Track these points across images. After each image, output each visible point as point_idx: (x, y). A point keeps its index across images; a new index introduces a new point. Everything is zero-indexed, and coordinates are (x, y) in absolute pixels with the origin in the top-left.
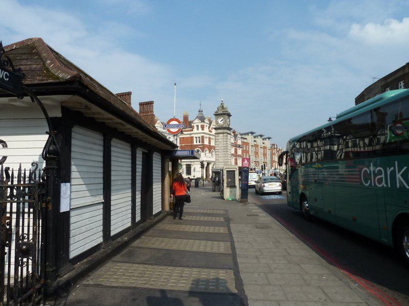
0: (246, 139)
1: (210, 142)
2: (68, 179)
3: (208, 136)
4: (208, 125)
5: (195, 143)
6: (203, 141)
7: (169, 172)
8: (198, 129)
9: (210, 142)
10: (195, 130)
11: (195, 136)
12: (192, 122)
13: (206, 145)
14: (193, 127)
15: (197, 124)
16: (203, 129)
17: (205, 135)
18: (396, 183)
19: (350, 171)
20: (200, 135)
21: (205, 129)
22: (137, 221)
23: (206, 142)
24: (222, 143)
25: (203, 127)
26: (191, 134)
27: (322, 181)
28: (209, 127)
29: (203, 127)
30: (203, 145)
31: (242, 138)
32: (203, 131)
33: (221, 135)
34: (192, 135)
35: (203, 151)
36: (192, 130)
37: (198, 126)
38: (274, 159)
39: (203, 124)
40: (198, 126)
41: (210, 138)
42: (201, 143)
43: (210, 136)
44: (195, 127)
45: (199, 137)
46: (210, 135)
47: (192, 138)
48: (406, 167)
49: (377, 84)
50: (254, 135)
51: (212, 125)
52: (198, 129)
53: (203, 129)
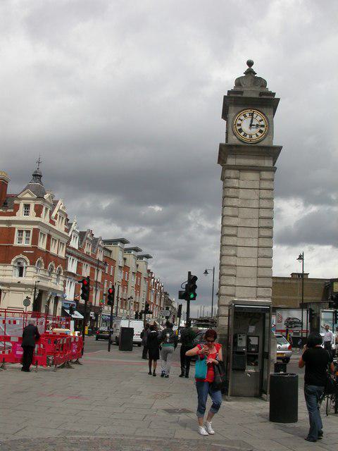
0: (110, 252)
1: (48, 246)
2: (225, 96)
5: (16, 243)
6: (35, 241)
8: (27, 213)
9: (48, 246)
10: (20, 215)
12: (15, 197)
13: (41, 251)
14: (16, 207)
15: (27, 202)
16: (38, 215)
20: (31, 227)
21: (43, 215)
22: (82, 317)
24: (255, 204)
25: (38, 211)
26: (9, 222)
29: (38, 211)
30: (35, 249)
31: (105, 249)
32: (38, 219)
33: (252, 176)
34: (13, 226)
35: (32, 263)
36: (14, 214)
37: (27, 206)
39: (39, 202)
40: (27, 206)
42: (29, 245)
43: (51, 233)
44: (22, 207)
45: (28, 232)
48: (188, 353)
50: (126, 246)
52: (27, 213)
53: (38, 215)
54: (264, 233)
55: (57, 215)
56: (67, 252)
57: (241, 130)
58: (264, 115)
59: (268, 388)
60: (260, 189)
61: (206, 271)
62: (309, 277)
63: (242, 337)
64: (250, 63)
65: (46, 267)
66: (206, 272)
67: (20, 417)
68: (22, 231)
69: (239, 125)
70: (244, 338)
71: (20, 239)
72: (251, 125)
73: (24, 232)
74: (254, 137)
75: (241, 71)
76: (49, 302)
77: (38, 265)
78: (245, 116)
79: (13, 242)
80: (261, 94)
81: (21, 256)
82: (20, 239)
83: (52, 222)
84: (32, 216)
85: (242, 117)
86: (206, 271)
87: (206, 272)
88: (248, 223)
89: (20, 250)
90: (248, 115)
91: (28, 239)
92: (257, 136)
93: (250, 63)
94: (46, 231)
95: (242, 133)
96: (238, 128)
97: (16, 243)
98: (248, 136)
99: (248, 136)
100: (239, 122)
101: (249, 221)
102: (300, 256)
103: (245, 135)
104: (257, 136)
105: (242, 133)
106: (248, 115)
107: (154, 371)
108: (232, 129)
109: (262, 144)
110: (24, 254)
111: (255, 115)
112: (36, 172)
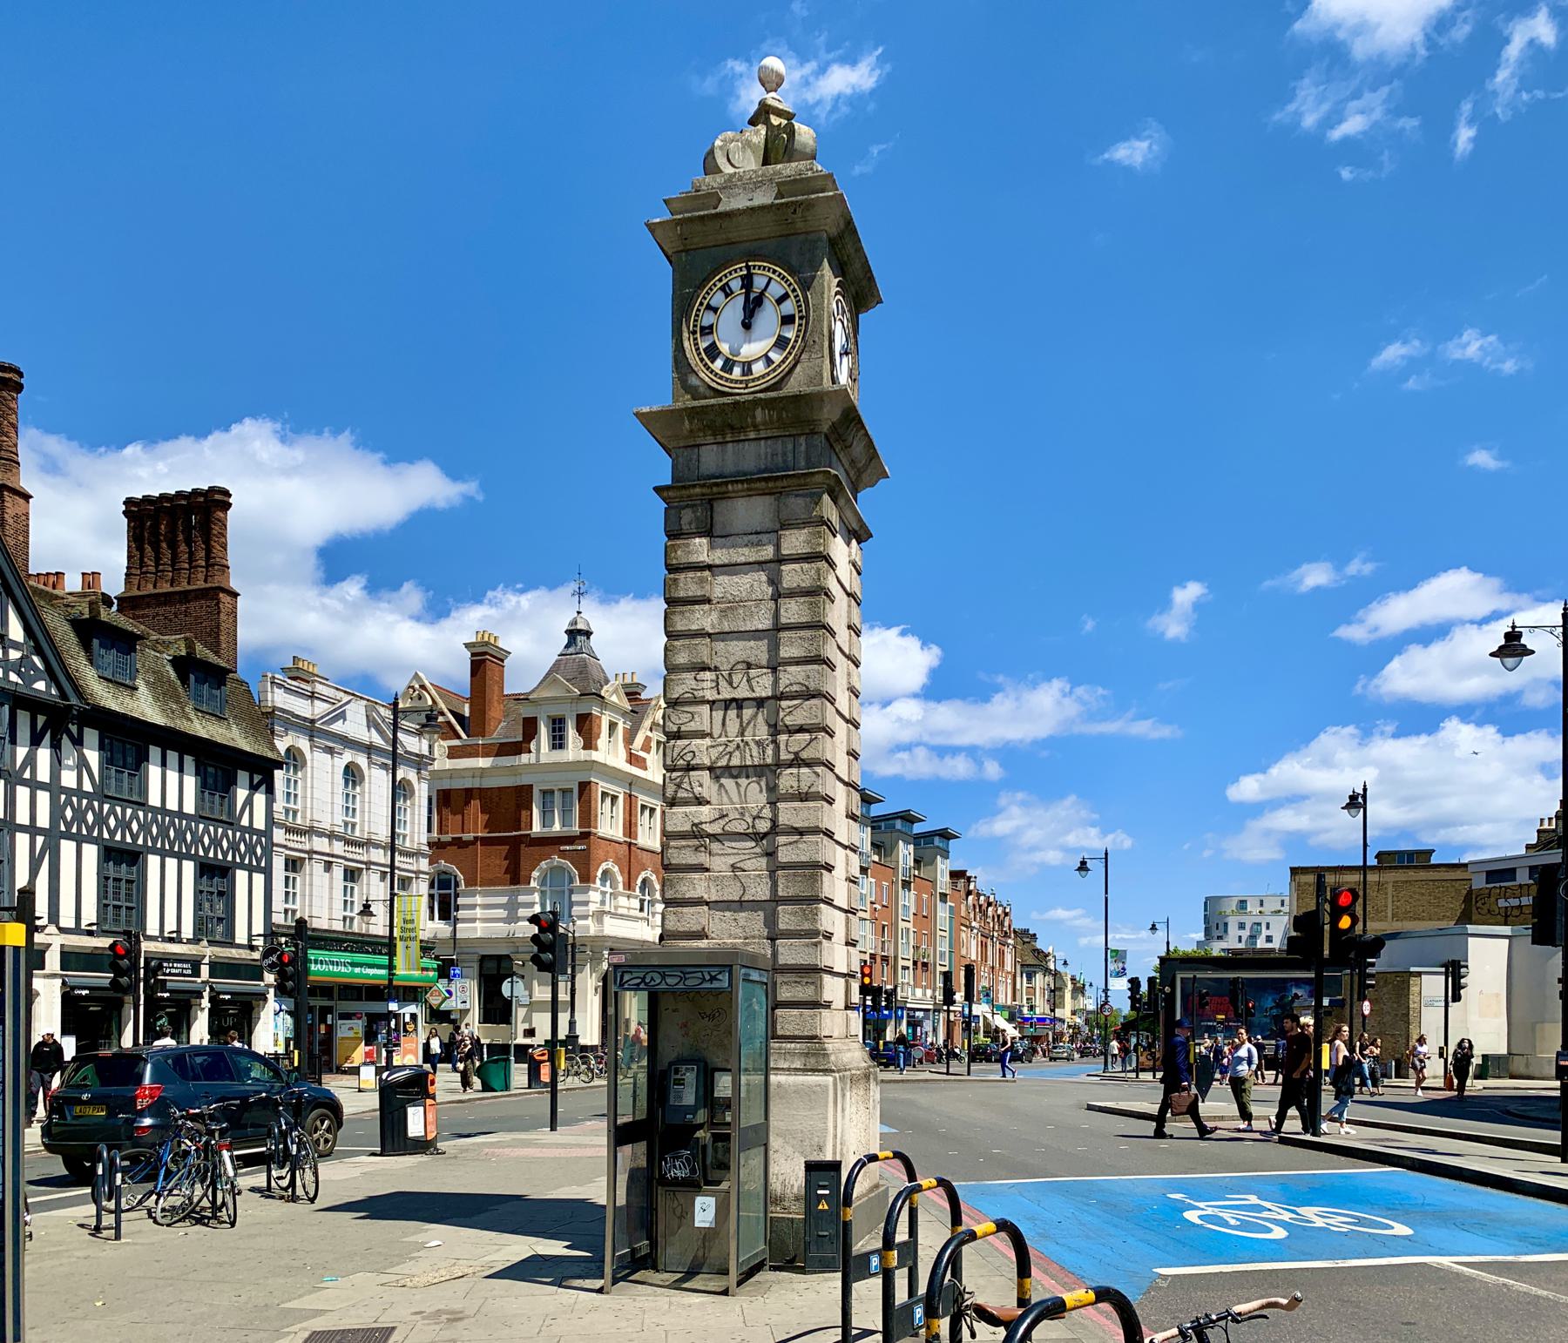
1: (630, 828)
6: (587, 817)
8: (558, 742)
9: (630, 828)
15: (556, 711)
16: (589, 744)
21: (602, 742)
34: (525, 781)
42: (576, 829)
52: (558, 742)
53: (589, 744)
55: (648, 739)
61: (1083, 863)
65: (629, 885)
68: (552, 792)
69: (708, 330)
73: (557, 795)
77: (642, 890)
78: (727, 291)
83: (633, 759)
84: (574, 748)
85: (718, 299)
97: (537, 828)
102: (1353, 798)
106: (736, 285)
107: (572, 1024)
109: (793, 386)
110: (563, 854)
111: (759, 283)
112: (575, 622)
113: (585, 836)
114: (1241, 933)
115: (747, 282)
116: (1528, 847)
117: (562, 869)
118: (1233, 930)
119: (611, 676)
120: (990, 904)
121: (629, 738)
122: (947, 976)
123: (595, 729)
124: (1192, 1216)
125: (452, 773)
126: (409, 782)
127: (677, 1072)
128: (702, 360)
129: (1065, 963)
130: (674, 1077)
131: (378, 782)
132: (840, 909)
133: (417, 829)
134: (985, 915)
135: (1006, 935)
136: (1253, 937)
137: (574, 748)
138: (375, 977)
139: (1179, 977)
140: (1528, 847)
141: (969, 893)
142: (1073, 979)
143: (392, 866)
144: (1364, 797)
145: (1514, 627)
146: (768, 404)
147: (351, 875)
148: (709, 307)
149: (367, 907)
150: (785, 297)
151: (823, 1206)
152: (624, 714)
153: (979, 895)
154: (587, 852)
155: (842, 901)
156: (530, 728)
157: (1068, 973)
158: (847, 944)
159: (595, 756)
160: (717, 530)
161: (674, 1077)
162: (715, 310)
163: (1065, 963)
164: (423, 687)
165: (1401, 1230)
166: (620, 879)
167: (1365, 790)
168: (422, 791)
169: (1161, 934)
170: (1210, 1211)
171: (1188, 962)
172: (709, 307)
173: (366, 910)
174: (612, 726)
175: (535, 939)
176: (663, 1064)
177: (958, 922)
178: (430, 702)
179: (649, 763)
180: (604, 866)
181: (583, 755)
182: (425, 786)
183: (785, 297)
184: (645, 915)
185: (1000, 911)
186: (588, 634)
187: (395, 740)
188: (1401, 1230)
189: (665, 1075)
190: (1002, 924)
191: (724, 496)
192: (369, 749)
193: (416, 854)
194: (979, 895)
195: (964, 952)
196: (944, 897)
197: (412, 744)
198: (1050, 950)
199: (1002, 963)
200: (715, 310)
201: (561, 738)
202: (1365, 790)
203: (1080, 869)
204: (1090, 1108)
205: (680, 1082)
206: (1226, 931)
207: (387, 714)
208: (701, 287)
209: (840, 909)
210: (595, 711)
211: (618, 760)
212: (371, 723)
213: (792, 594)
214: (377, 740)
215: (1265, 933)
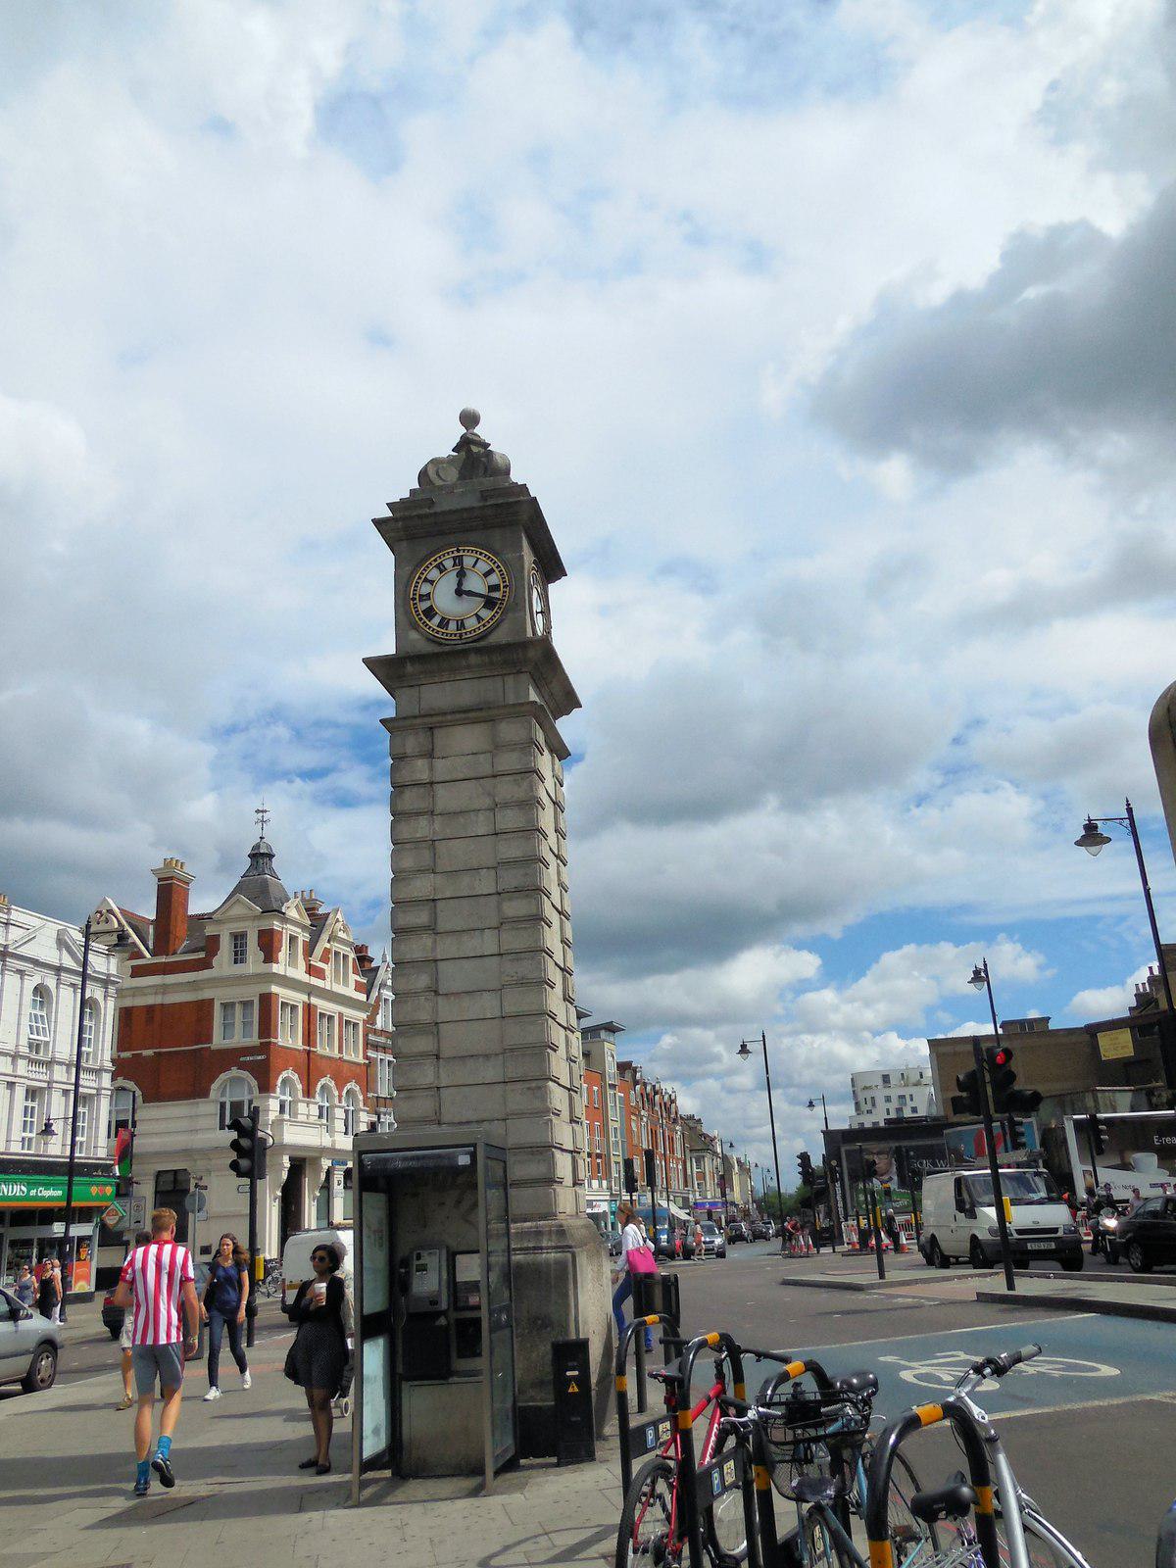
3: (298, 998)
4: (303, 937)
5: (218, 1041)
6: (266, 1027)
7: (351, 1336)
8: (239, 956)
9: (309, 1038)
11: (219, 995)
15: (238, 927)
17: (322, 1005)
18: (109, 1483)
19: (321, 1039)
20: (252, 993)
21: (283, 955)
23: (287, 1037)
26: (194, 985)
27: (517, 1386)
28: (309, 950)
34: (206, 994)
36: (205, 964)
38: (635, 1142)
40: (239, 939)
41: (309, 1008)
42: (254, 1040)
43: (314, 1001)
45: (247, 1004)
46: (311, 990)
47: (204, 1008)
49: (1061, 1033)
51: (325, 936)
52: (239, 956)
53: (270, 957)
54: (515, 908)
56: (367, 1044)
57: (430, 613)
58: (496, 554)
59: (1085, 1363)
60: (495, 776)
61: (744, 1046)
62: (1052, 1026)
63: (426, 1259)
64: (469, 419)
66: (744, 1050)
67: (431, 1528)
68: (233, 1004)
70: (434, 1261)
71: (228, 1027)
72: (459, 592)
73: (238, 1008)
74: (471, 624)
75: (444, 442)
76: (327, 1187)
78: (441, 568)
79: (209, 1039)
80: (484, 495)
81: (234, 1072)
82: (228, 1027)
83: (310, 970)
84: (254, 962)
85: (434, 574)
86: (744, 1046)
87: (744, 1050)
88: (464, 885)
89: (230, 1058)
90: (449, 564)
91: (246, 1024)
92: (479, 618)
93: (469, 419)
94: (298, 998)
95: (437, 620)
96: (425, 605)
97: (218, 1041)
98: (452, 626)
99: (452, 626)
100: (425, 589)
101: (466, 879)
102: (977, 972)
103: (444, 623)
104: (479, 618)
105: (437, 620)
106: (449, 564)
108: (410, 605)
109: (493, 639)
110: (242, 1066)
111: (468, 561)
112: (257, 847)
113: (265, 1048)
114: (888, 1105)
115: (458, 561)
116: (1131, 1009)
117: (239, 1080)
118: (881, 1105)
119: (291, 895)
120: (656, 1093)
121: (309, 950)
122: (628, 1164)
123: (276, 944)
124: (907, 1376)
125: (136, 991)
126: (96, 1002)
127: (419, 1257)
128: (421, 619)
129: (731, 1146)
130: (416, 1263)
131: (66, 1001)
132: (564, 1087)
133: (103, 1048)
134: (653, 1104)
135: (675, 1121)
136: (899, 1110)
137: (254, 962)
138: (51, 1198)
139: (843, 1150)
140: (1131, 1009)
141: (636, 1083)
142: (739, 1161)
143: (77, 1085)
144: (986, 971)
145: (1090, 820)
146: (479, 651)
147: (32, 1093)
148: (426, 580)
149: (48, 1126)
150: (491, 571)
151: (574, 1389)
152: (304, 928)
153: (645, 1084)
154: (266, 1064)
155: (565, 1081)
156: (212, 945)
157: (734, 1156)
158: (572, 1121)
159: (276, 968)
160: (437, 753)
161: (416, 1263)
162: (432, 582)
163: (731, 1146)
164: (110, 911)
165: (1107, 1371)
166: (299, 1087)
167: (985, 965)
168: (109, 1010)
169: (819, 1109)
170: (924, 1370)
171: (848, 1136)
172: (426, 580)
173: (47, 1130)
174: (293, 939)
175: (235, 1145)
176: (403, 1251)
177: (630, 1112)
178: (116, 925)
179: (327, 973)
180: (284, 1074)
181: (263, 968)
182: (111, 1004)
183: (491, 571)
184: (324, 1121)
185: (666, 1098)
186: (271, 856)
187: (85, 964)
188: (1107, 1371)
189: (406, 1263)
190: (668, 1111)
191: (442, 726)
192: (58, 970)
193: (98, 1072)
194: (645, 1084)
195: (635, 1142)
196: (613, 1086)
197: (99, 964)
198: (716, 1133)
199: (672, 1151)
200: (432, 582)
201: (243, 953)
202: (985, 965)
203: (740, 1052)
204: (786, 1283)
205: (423, 1268)
206: (874, 1105)
207: (80, 938)
208: (419, 565)
209: (564, 1087)
210: (277, 925)
211: (299, 973)
212: (61, 943)
213: (506, 805)
214: (68, 962)
215: (910, 1104)
